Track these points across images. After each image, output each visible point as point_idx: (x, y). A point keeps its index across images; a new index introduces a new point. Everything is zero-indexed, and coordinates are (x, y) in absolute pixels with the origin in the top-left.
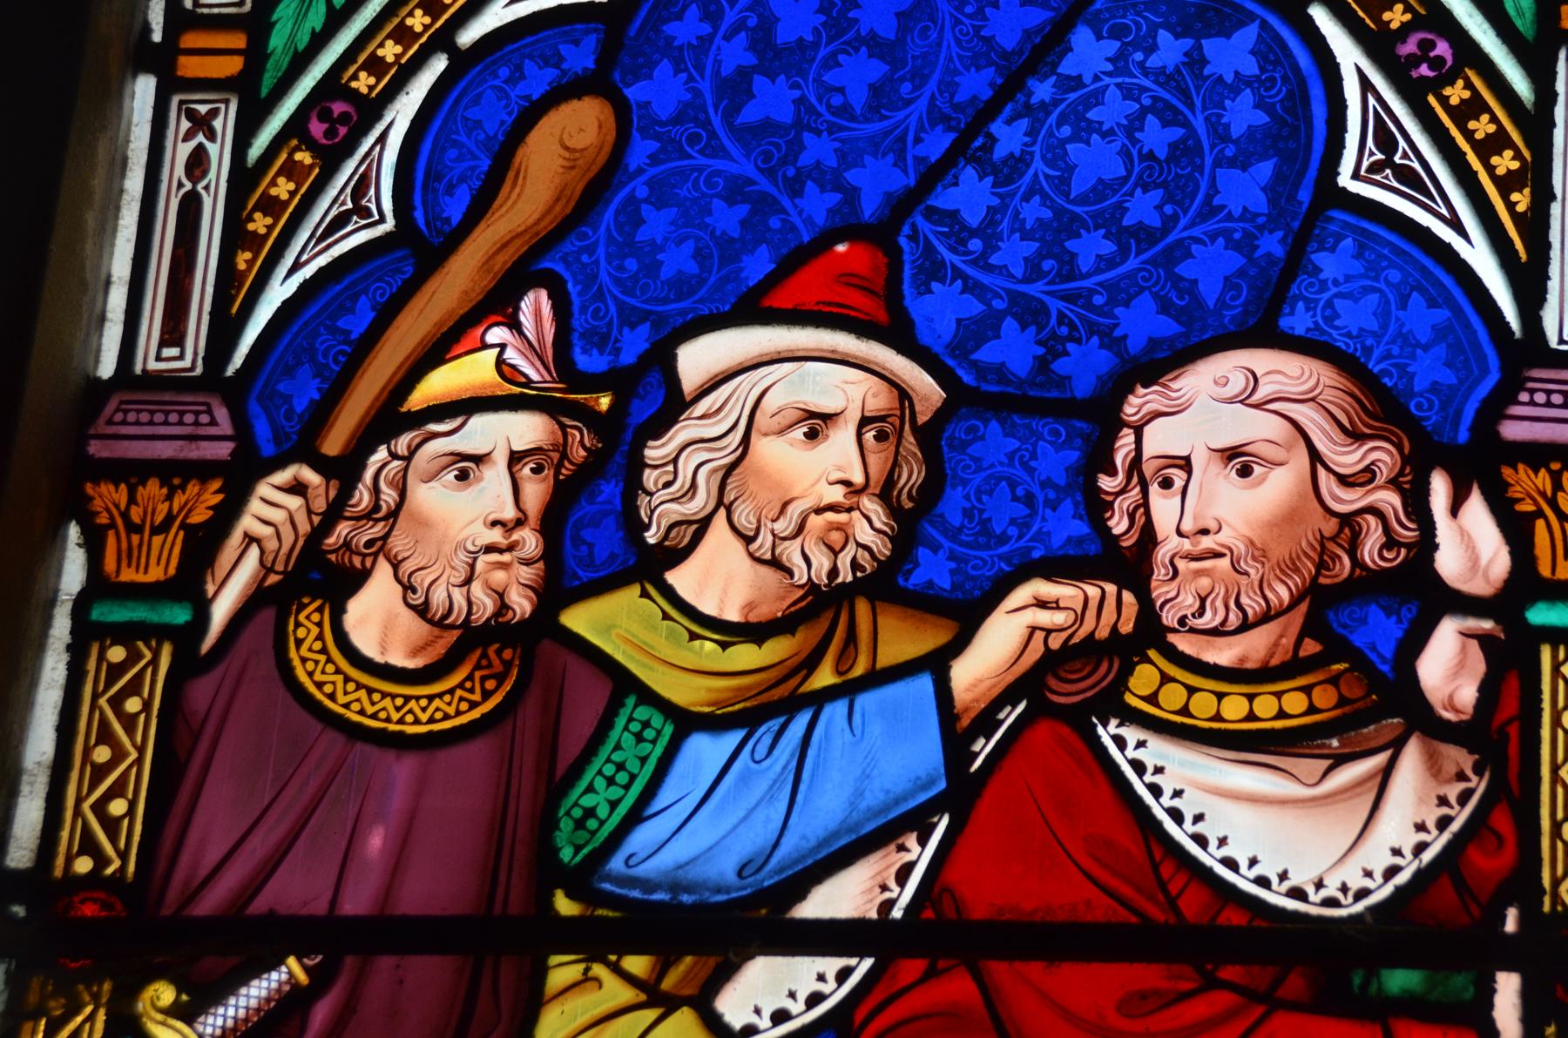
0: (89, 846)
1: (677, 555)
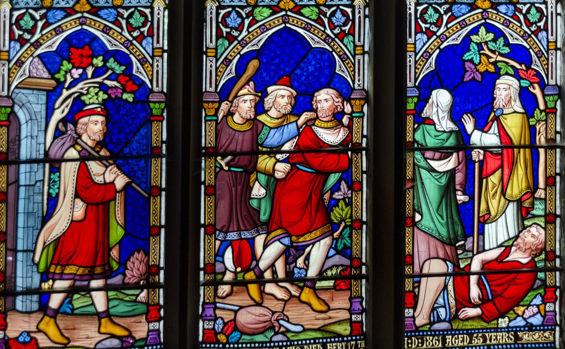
0: (210, 143)
1: (268, 111)
